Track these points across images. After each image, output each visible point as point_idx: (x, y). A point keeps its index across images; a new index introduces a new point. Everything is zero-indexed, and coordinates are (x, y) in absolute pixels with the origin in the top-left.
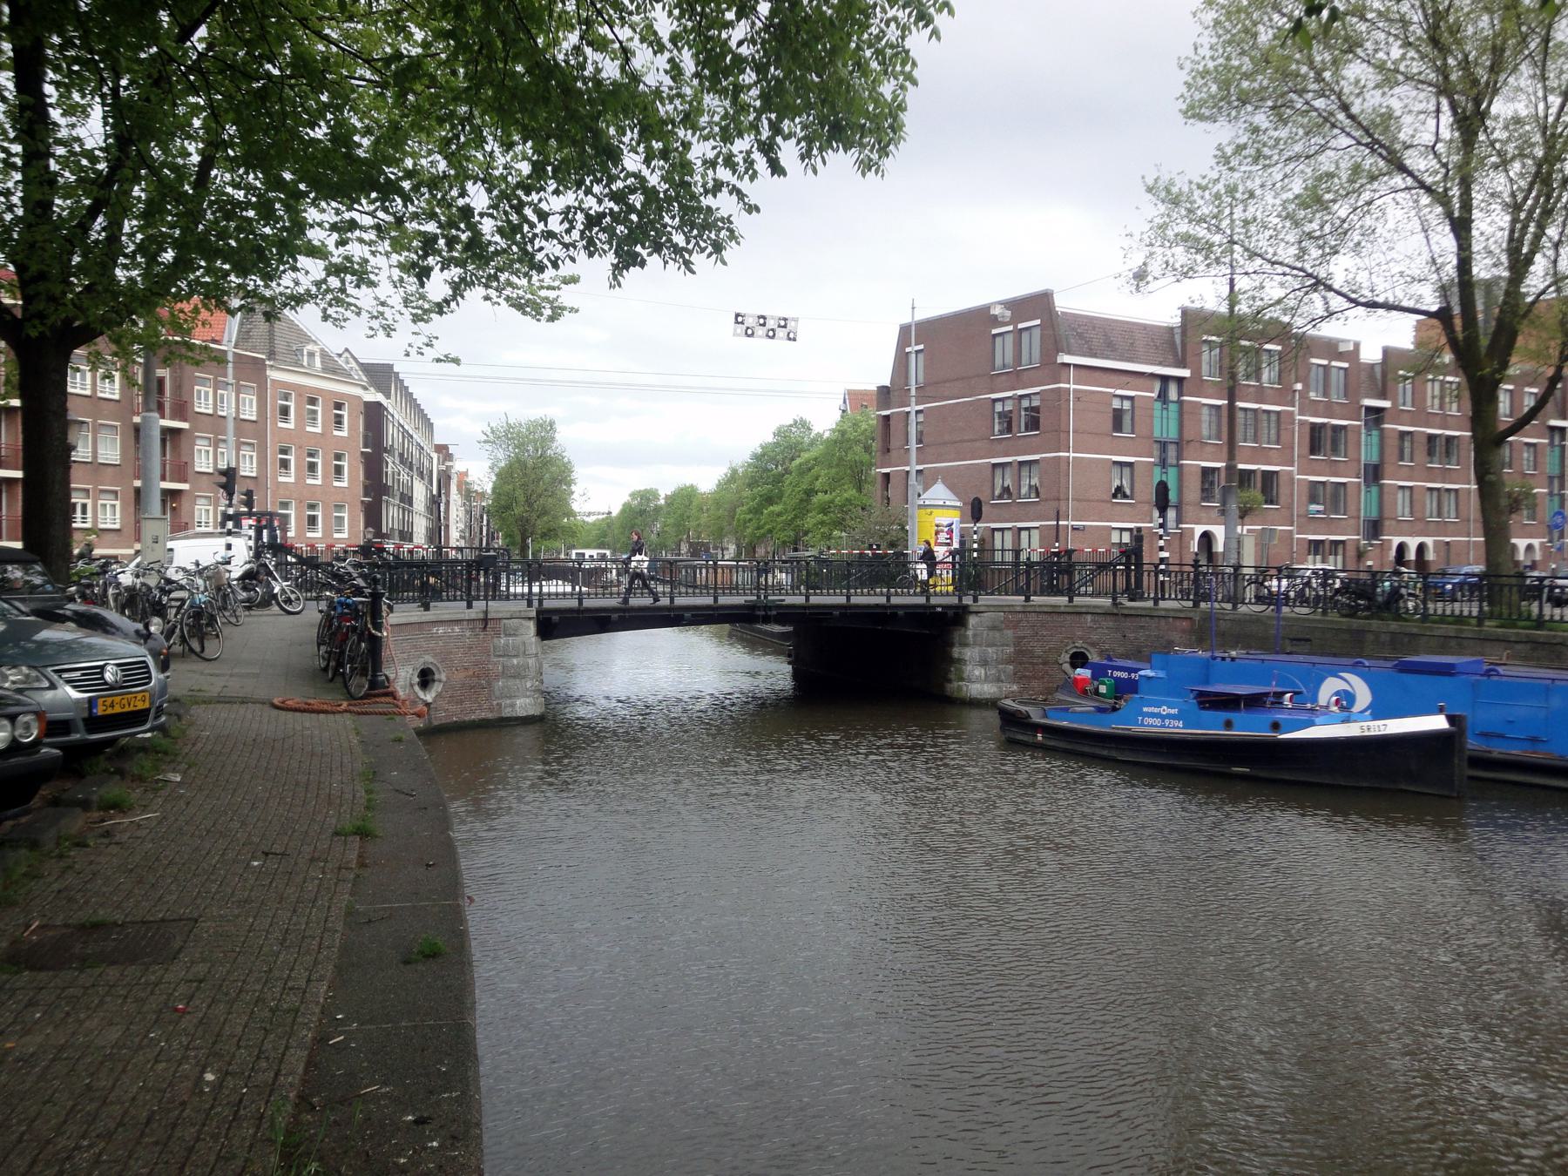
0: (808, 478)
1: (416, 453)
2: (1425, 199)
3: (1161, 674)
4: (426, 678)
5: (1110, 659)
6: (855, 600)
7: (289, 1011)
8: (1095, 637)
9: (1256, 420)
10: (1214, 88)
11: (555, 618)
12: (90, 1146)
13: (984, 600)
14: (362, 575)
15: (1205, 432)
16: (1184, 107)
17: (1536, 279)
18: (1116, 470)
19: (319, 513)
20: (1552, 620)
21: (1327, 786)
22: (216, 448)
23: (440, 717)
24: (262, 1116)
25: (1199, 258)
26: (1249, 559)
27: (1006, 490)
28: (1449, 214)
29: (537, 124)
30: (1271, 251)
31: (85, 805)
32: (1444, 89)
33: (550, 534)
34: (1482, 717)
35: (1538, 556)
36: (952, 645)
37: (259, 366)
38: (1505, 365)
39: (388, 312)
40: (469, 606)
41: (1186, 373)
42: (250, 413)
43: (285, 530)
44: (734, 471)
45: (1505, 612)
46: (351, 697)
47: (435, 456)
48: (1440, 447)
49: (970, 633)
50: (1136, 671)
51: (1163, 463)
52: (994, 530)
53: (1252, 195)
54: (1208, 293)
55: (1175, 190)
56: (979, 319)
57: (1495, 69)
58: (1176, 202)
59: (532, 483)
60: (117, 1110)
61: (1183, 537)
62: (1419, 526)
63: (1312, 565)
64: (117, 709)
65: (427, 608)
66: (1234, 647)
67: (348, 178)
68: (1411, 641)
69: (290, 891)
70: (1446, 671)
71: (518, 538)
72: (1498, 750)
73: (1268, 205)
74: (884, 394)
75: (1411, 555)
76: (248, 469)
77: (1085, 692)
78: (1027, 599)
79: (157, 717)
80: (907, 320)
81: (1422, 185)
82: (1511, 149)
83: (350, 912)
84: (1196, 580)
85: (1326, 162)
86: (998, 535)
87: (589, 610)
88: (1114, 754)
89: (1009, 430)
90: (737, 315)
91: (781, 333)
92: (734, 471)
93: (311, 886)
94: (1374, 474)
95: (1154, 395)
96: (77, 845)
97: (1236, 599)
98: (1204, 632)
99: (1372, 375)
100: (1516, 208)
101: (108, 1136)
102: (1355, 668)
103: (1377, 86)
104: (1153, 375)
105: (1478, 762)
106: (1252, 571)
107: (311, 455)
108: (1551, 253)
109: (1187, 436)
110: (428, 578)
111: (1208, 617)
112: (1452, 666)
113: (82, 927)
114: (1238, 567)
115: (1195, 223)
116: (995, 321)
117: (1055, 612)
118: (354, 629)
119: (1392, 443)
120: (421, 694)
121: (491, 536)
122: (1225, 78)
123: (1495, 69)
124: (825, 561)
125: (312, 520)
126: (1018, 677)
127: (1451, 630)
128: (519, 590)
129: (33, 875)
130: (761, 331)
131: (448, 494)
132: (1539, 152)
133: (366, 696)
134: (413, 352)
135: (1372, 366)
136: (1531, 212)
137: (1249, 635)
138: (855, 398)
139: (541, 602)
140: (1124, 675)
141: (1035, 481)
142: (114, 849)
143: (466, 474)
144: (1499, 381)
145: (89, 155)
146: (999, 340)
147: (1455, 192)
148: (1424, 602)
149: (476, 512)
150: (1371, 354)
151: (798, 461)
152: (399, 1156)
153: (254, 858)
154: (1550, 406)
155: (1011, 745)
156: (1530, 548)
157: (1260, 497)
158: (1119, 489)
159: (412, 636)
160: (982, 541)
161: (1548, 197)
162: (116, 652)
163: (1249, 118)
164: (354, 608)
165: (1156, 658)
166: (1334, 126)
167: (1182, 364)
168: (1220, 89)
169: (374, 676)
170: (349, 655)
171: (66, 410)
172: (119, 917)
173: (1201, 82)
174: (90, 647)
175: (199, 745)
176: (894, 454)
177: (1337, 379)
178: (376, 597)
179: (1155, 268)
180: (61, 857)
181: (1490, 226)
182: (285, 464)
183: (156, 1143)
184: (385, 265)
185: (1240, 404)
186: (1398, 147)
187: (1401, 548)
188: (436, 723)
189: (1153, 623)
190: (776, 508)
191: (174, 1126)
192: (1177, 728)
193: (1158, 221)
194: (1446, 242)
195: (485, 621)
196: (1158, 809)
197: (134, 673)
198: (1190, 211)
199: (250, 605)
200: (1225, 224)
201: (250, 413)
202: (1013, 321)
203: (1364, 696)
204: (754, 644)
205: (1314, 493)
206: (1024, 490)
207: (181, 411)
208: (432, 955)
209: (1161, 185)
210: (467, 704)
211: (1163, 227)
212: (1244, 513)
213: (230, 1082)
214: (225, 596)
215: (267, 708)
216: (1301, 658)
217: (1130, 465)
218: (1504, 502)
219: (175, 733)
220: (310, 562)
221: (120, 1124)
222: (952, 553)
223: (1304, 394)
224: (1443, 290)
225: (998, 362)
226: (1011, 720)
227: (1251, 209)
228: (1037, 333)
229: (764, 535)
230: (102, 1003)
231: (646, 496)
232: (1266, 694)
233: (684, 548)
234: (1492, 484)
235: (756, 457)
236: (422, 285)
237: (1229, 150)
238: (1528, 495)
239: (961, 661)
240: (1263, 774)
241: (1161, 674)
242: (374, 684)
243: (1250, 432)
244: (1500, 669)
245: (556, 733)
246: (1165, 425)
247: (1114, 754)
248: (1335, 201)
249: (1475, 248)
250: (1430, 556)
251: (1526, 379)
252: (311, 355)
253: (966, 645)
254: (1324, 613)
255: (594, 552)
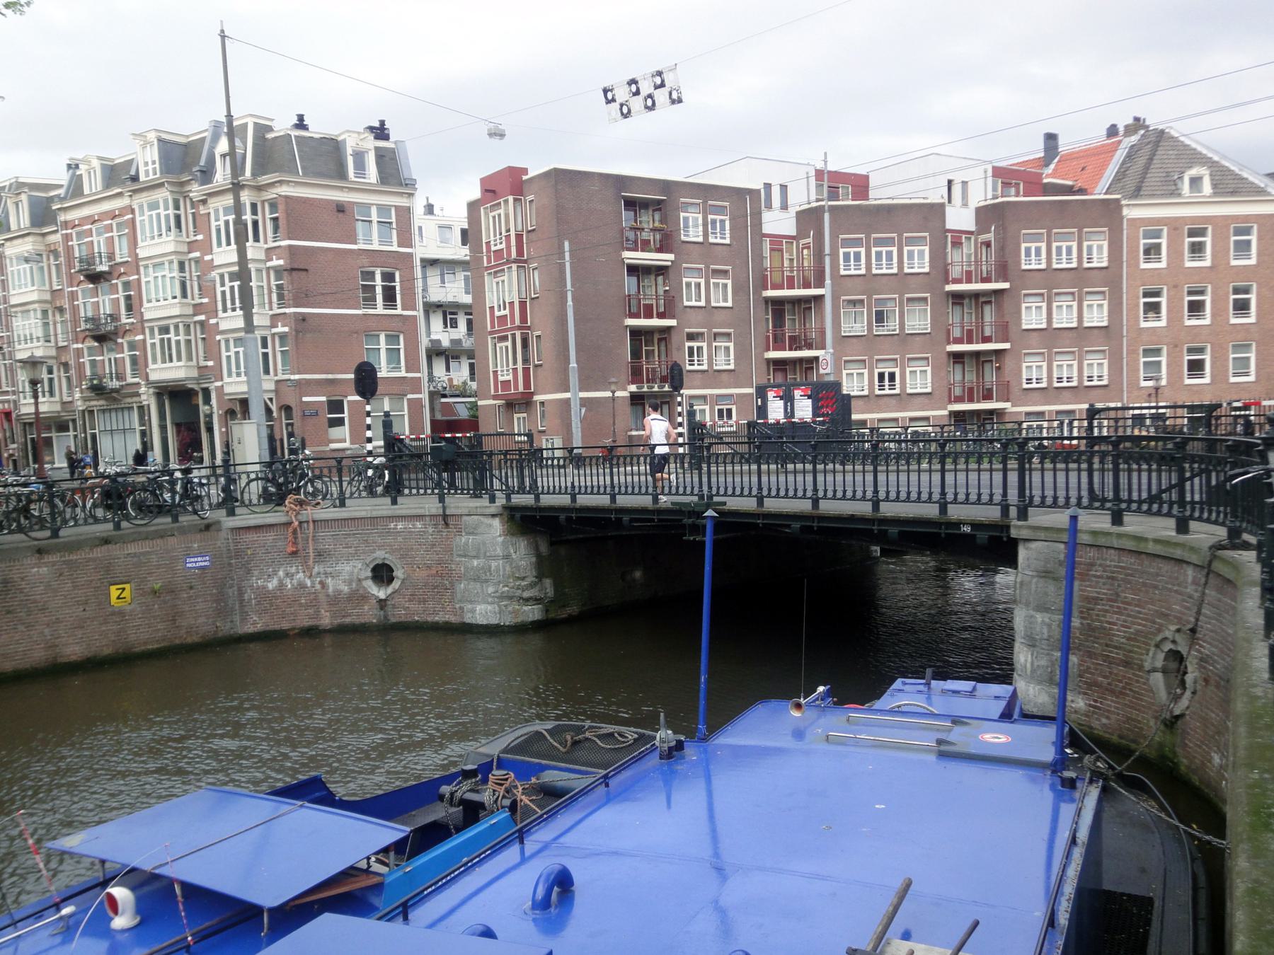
23: (398, 614)
90: (605, 91)
188: (393, 620)
210: (431, 605)
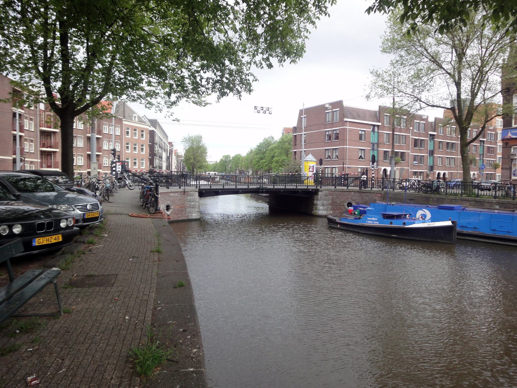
0: (272, 152)
1: (163, 145)
2: (448, 76)
3: (373, 209)
4: (168, 208)
5: (358, 204)
6: (287, 187)
7: (145, 300)
8: (354, 198)
9: (399, 137)
10: (390, 44)
11: (204, 191)
12: (99, 335)
13: (323, 188)
14: (151, 179)
15: (385, 141)
16: (382, 49)
17: (478, 100)
18: (360, 151)
19: (137, 161)
20: (481, 195)
21: (418, 240)
22: (109, 143)
23: (172, 218)
24: (142, 329)
25: (385, 92)
26: (397, 177)
27: (329, 157)
28: (455, 81)
29: (203, 55)
30: (405, 90)
31: (84, 243)
32: (454, 46)
33: (200, 167)
34: (462, 222)
35: (476, 177)
36: (314, 200)
37: (121, 120)
38: (469, 124)
39: (160, 106)
40: (180, 188)
41: (380, 124)
42: (118, 133)
43: (128, 166)
44: (252, 150)
45: (468, 192)
46: (150, 213)
47: (168, 145)
48: (450, 145)
49: (319, 197)
50: (366, 208)
51: (373, 149)
52: (325, 168)
53: (400, 75)
54: (387, 102)
55: (378, 73)
56: (321, 109)
57: (467, 41)
58: (378, 76)
59: (195, 153)
60: (104, 326)
61: (378, 170)
62: (444, 168)
63: (414, 178)
64: (91, 217)
65: (168, 188)
66: (393, 202)
67: (154, 69)
68: (442, 200)
69: (141, 267)
70: (452, 209)
71: (191, 168)
72: (465, 231)
73: (404, 78)
74: (295, 129)
75: (442, 176)
76: (118, 149)
77: (351, 214)
78: (335, 187)
79: (101, 219)
80: (302, 108)
81: (448, 73)
82: (471, 63)
83: (158, 274)
84: (383, 183)
85: (420, 66)
86: (326, 169)
87: (213, 189)
88: (359, 231)
89: (330, 139)
91: (267, 112)
92: (252, 150)
93: (146, 266)
94: (432, 153)
95: (371, 130)
96: (83, 253)
97: (393, 188)
98: (385, 197)
99: (431, 126)
100: (473, 79)
101: (103, 332)
102: (426, 208)
103: (435, 45)
104: (371, 125)
105: (459, 234)
106: (398, 180)
107: (127, 144)
108: (483, 92)
109: (380, 142)
110: (169, 180)
111: (386, 193)
112: (453, 207)
113: (87, 276)
114: (394, 179)
115: (385, 83)
116: (327, 109)
117: (343, 191)
118: (151, 195)
119: (437, 144)
120: (167, 212)
121: (184, 168)
122: (393, 41)
123: (467, 41)
124: (278, 176)
125: (135, 163)
126: (333, 209)
127: (453, 197)
128: (194, 183)
129: (72, 262)
130: (262, 111)
131: (172, 156)
132: (480, 64)
133: (154, 213)
134: (167, 117)
135: (432, 123)
136: (477, 81)
137: (397, 198)
138: (286, 130)
139: (200, 187)
140: (363, 209)
141: (337, 154)
142: (93, 255)
143: (177, 150)
144: (468, 128)
145: (79, 63)
146: (327, 114)
147: (456, 75)
148: (446, 189)
149: (180, 161)
150: (431, 119)
151: (270, 147)
152: (180, 340)
153: (130, 258)
154: (481, 136)
155: (331, 228)
156: (474, 174)
157: (400, 159)
158: (361, 157)
159: (166, 195)
160: (322, 171)
161: (482, 77)
162: (89, 200)
163: (400, 53)
164: (151, 189)
165: (371, 204)
166: (423, 55)
167: (379, 121)
168: (392, 44)
169: (156, 207)
170: (149, 201)
171: (73, 134)
172: (96, 274)
173: (386, 42)
174: (81, 199)
175: (111, 227)
176: (297, 146)
177: (422, 126)
178: (157, 186)
179: (373, 94)
180: (79, 257)
181: (466, 85)
182: (128, 147)
183: (116, 335)
184: (162, 92)
185: (395, 133)
186: (440, 62)
187: (439, 174)
189: (370, 195)
190: (264, 161)
191: (120, 330)
192: (377, 224)
193: (374, 81)
194: (454, 89)
195: (184, 192)
196: (370, 247)
197: (95, 207)
198: (383, 79)
199: (120, 187)
200: (392, 83)
201: (118, 133)
202: (332, 109)
203: (429, 215)
204: (257, 199)
205: (415, 158)
206: (334, 156)
207: (100, 132)
208: (181, 286)
209: (374, 71)
211: (375, 83)
212: (396, 164)
213: (133, 319)
214: (114, 184)
215: (128, 216)
216: (412, 205)
217: (364, 150)
218: (469, 162)
219: (104, 223)
220: (134, 175)
221: (106, 330)
222: (314, 174)
223: (413, 130)
224: (452, 102)
225: (327, 120)
226: (331, 221)
227: (399, 78)
228: (338, 112)
229: (260, 169)
230: (96, 297)
231: (227, 157)
232: (402, 215)
233: (237, 172)
234: (466, 157)
235: (258, 146)
236: (170, 98)
237: (394, 62)
238: (475, 160)
239: (316, 205)
240: (400, 237)
241: (373, 209)
242: (156, 210)
243: (398, 140)
244: (466, 208)
245: (203, 223)
246: (374, 139)
247: (359, 231)
248: (423, 77)
249: (462, 90)
250: (447, 176)
251: (474, 127)
252: (135, 117)
253: (318, 200)
254: (418, 192)
255: (213, 173)
